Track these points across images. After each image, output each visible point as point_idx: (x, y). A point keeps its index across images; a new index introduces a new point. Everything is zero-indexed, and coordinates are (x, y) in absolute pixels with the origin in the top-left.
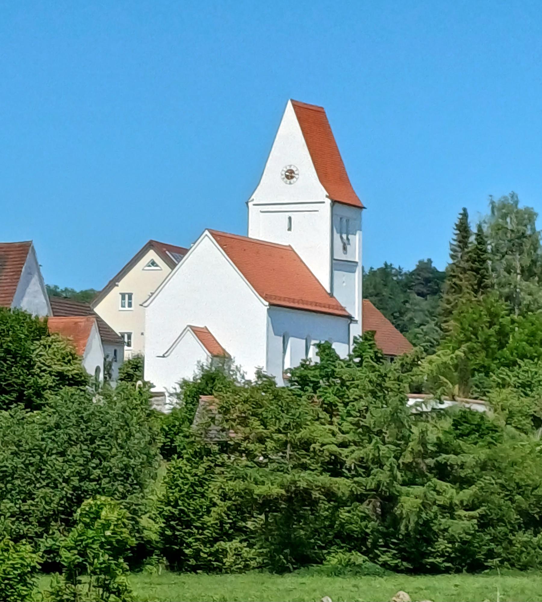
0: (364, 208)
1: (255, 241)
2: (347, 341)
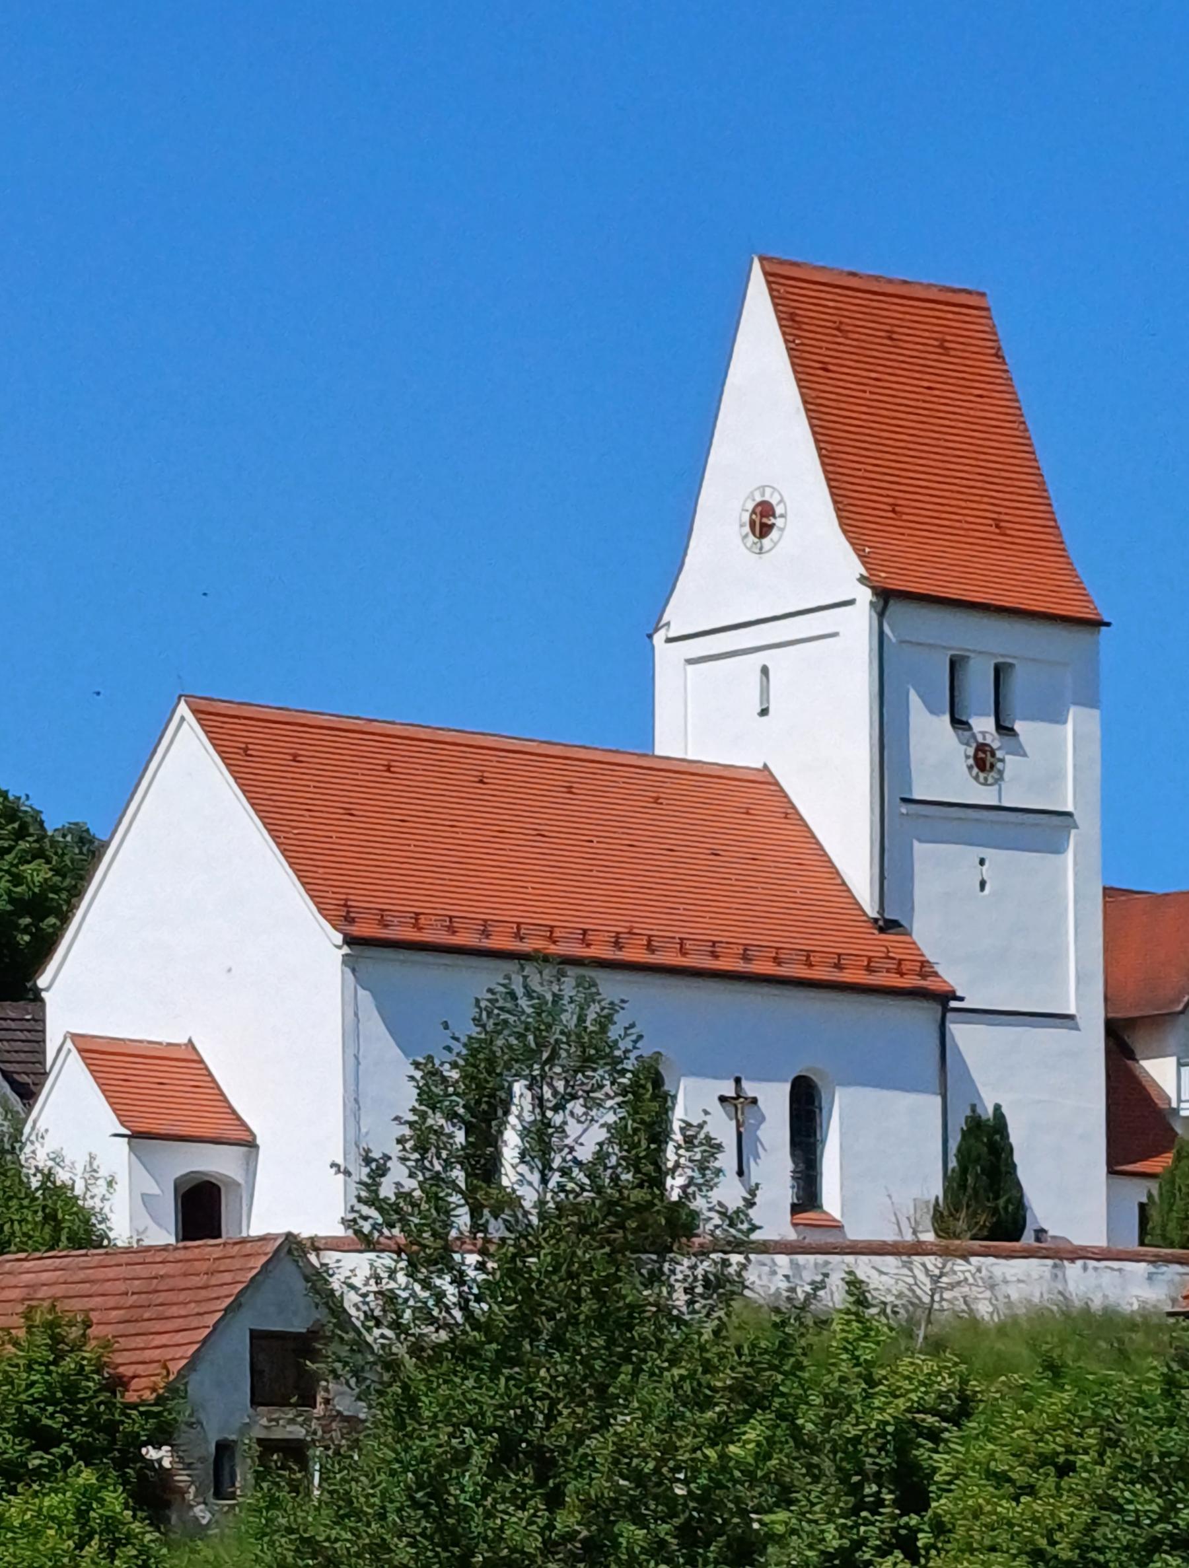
0: (1108, 624)
1: (683, 767)
2: (935, 1082)
